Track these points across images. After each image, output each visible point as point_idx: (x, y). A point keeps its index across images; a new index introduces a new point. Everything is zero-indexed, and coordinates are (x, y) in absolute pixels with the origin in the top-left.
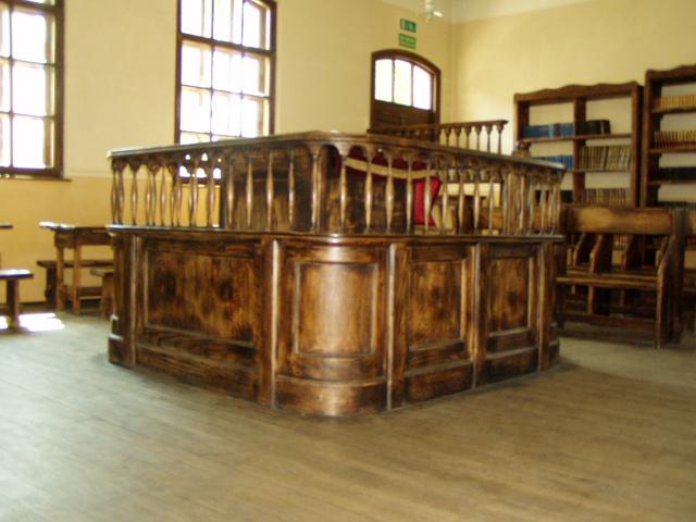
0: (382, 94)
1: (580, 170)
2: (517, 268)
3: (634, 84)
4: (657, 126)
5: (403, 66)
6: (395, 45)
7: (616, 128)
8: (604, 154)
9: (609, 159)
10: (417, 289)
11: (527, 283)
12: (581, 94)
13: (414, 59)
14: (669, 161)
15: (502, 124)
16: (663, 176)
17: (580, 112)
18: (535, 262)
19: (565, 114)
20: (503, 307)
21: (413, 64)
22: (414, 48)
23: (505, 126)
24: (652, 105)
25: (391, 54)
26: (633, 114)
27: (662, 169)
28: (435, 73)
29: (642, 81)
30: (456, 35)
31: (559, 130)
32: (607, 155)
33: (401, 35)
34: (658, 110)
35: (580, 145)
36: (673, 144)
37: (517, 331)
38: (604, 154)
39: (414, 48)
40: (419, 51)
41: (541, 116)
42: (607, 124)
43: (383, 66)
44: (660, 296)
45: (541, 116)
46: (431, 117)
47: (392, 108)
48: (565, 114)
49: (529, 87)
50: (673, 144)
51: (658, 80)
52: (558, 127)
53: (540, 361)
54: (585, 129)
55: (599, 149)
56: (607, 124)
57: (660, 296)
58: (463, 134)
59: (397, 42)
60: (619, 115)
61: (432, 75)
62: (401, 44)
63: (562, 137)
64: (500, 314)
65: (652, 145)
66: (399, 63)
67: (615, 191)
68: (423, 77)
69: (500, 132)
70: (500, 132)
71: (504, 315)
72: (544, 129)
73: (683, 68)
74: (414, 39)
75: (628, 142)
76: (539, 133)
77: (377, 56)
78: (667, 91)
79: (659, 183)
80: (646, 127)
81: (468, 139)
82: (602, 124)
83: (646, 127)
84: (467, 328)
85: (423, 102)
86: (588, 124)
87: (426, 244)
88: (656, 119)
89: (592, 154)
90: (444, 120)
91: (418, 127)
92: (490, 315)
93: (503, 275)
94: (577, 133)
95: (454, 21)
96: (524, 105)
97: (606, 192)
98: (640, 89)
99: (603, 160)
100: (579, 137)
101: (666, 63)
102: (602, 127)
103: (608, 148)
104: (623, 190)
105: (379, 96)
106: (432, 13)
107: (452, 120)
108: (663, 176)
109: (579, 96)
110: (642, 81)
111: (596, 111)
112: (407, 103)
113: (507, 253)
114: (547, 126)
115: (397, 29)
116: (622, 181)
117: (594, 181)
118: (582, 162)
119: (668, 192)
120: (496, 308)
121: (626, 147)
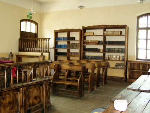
0: (23, 30)
1: (68, 48)
2: (37, 90)
3: (80, 29)
4: (85, 39)
5: (28, 23)
6: (26, 18)
7: (76, 39)
8: (74, 45)
9: (75, 46)
10: (3, 104)
11: (40, 92)
12: (69, 31)
13: (31, 21)
14: (87, 47)
15: (49, 39)
16: (86, 50)
17: (69, 35)
18: (42, 87)
19: (65, 35)
20: (33, 100)
21: (31, 22)
22: (31, 19)
23: (50, 39)
24: (84, 34)
25: (26, 20)
26: (80, 36)
27: (86, 48)
28: (37, 24)
29: (81, 29)
30: (42, 16)
31: (64, 39)
32: (74, 45)
33: (28, 16)
34: (84, 36)
35: (68, 42)
36: (88, 43)
37: (37, 105)
38: (74, 45)
39: (31, 19)
40: (32, 19)
41: (60, 35)
42: (74, 38)
43: (23, 23)
44: (78, 87)
45: (60, 35)
46: (36, 35)
47: (26, 33)
48: (65, 35)
49: (57, 29)
50: (88, 43)
51: (85, 29)
52: (64, 38)
53: (45, 111)
54: (70, 39)
55: (73, 43)
56: (74, 38)
57: (78, 87)
58: (40, 41)
59: (27, 17)
60: (77, 36)
61: (36, 25)
62: (28, 18)
63: (65, 40)
64: (32, 103)
65: (84, 43)
66: (28, 22)
67: (76, 53)
68: (34, 25)
69: (49, 41)
70: (49, 41)
71: (33, 102)
72: (61, 38)
73: (90, 26)
74: (31, 16)
75: (79, 42)
76: (60, 39)
77: (21, 21)
78: (87, 31)
79: (85, 52)
80: (82, 39)
81: (44, 42)
82: (73, 38)
83: (82, 39)
84: (20, 110)
85: (34, 31)
86: (70, 38)
87: (5, 92)
88: (85, 37)
89: (71, 44)
90: (39, 37)
91: (31, 39)
92: (28, 103)
93: (32, 92)
94: (68, 40)
95: (41, 12)
96: (56, 33)
97: (74, 53)
98: (81, 30)
99: (73, 46)
100: (68, 41)
101: (86, 25)
102: (74, 39)
103: (74, 43)
104: (78, 53)
105: (22, 30)
106: (33, 12)
107: (41, 37)
108: (86, 50)
109: (69, 31)
110: (81, 29)
111: (72, 35)
112: (29, 31)
113: (33, 87)
114: (61, 38)
115: (27, 14)
116: (77, 51)
117: (72, 51)
118: (69, 46)
119: (88, 54)
120: (30, 101)
121: (78, 43)
